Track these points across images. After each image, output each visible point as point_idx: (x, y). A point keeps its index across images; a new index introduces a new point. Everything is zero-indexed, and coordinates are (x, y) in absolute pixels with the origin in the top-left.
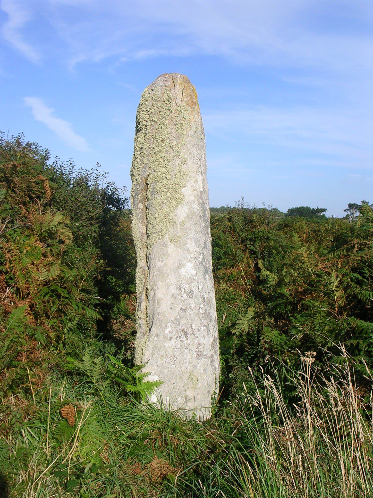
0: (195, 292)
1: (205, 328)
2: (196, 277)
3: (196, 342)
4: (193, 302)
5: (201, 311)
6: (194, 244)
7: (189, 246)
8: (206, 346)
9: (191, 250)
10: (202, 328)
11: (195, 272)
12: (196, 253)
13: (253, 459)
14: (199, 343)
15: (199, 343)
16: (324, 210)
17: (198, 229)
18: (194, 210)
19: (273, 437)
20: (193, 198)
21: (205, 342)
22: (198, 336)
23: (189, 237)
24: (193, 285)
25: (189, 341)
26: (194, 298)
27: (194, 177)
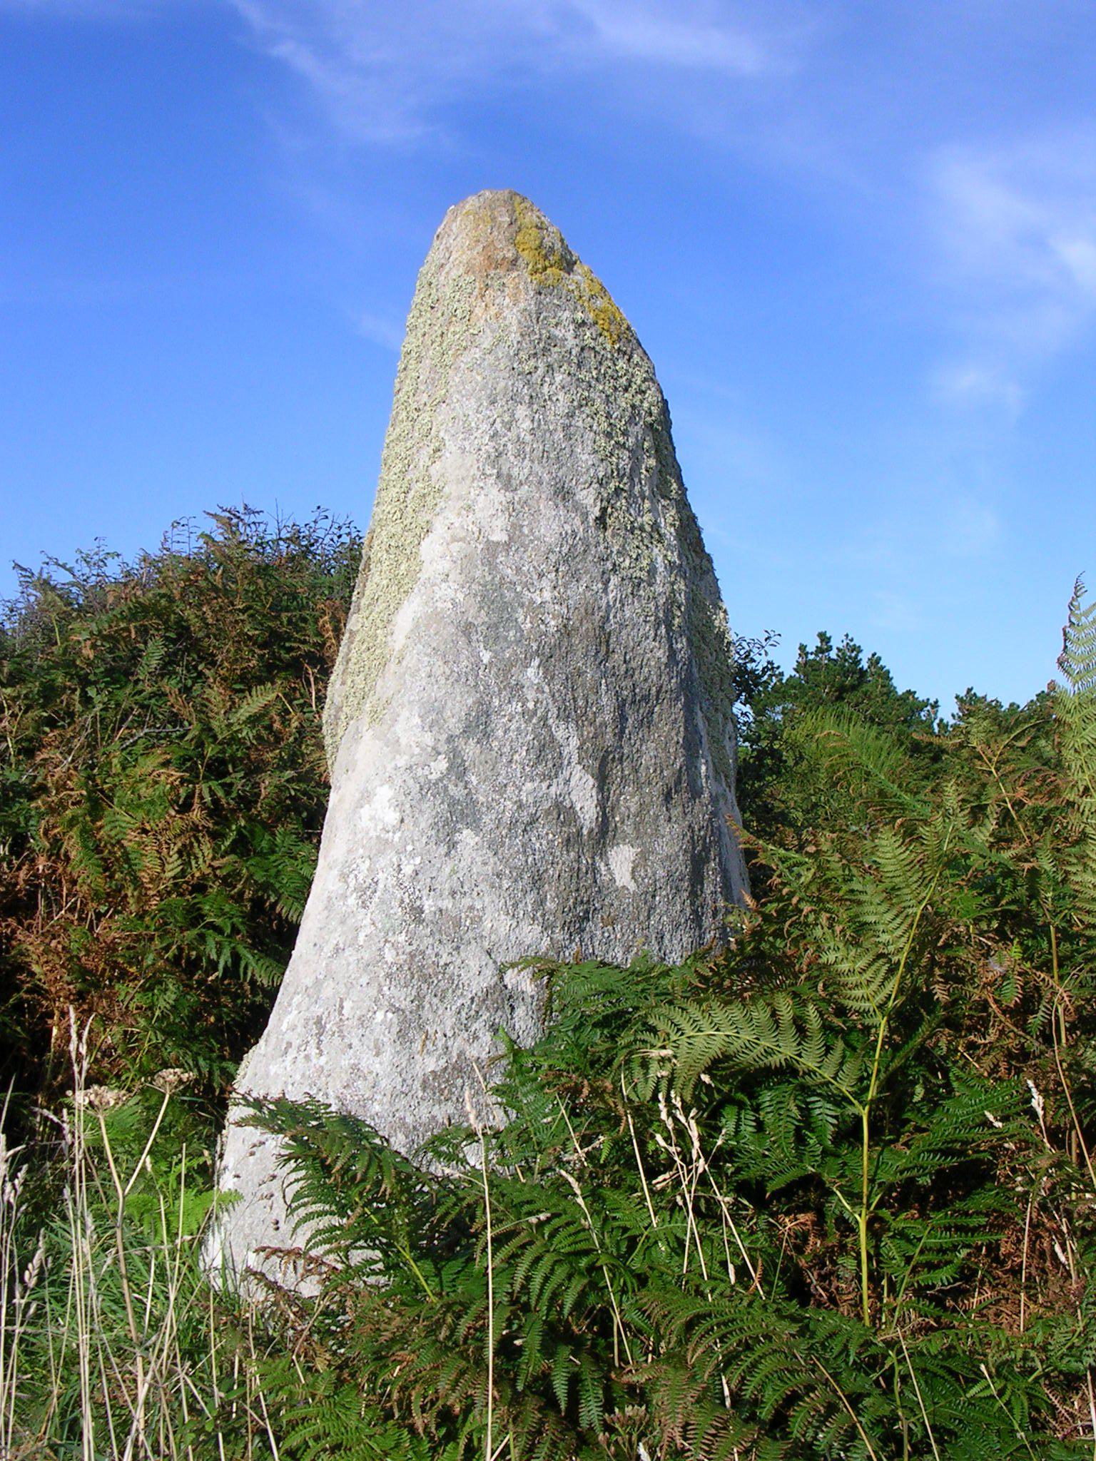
0: (381, 886)
1: (390, 1015)
2: (398, 834)
3: (345, 1062)
4: (367, 921)
5: (389, 956)
6: (417, 720)
7: (399, 728)
8: (383, 1083)
9: (403, 741)
10: (380, 1016)
11: (398, 816)
12: (417, 751)
13: (1079, 1145)
14: (355, 1068)
15: (355, 1068)
16: (802, 648)
17: (439, 668)
18: (438, 604)
19: (134, 1401)
20: (445, 565)
21: (377, 1068)
22: (355, 1042)
23: (405, 699)
24: (383, 862)
25: (323, 1060)
26: (372, 907)
27: (459, 498)
